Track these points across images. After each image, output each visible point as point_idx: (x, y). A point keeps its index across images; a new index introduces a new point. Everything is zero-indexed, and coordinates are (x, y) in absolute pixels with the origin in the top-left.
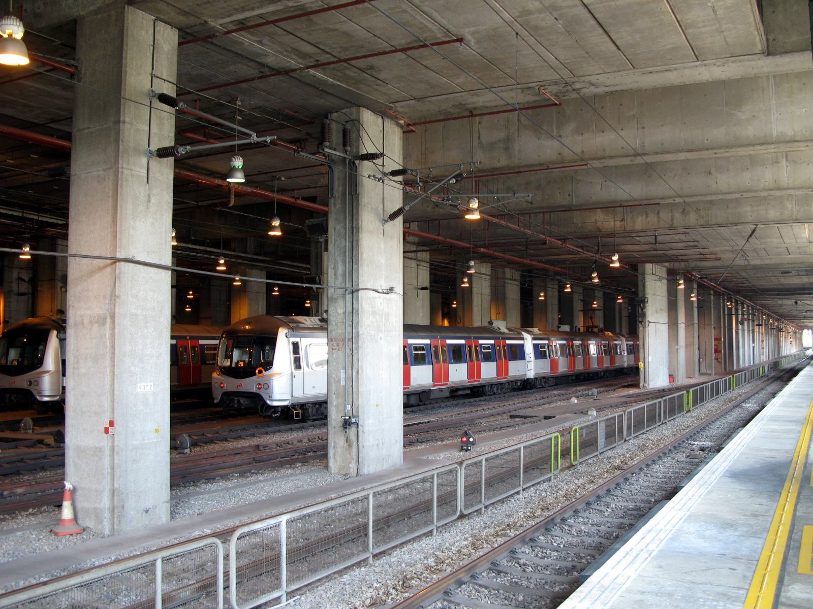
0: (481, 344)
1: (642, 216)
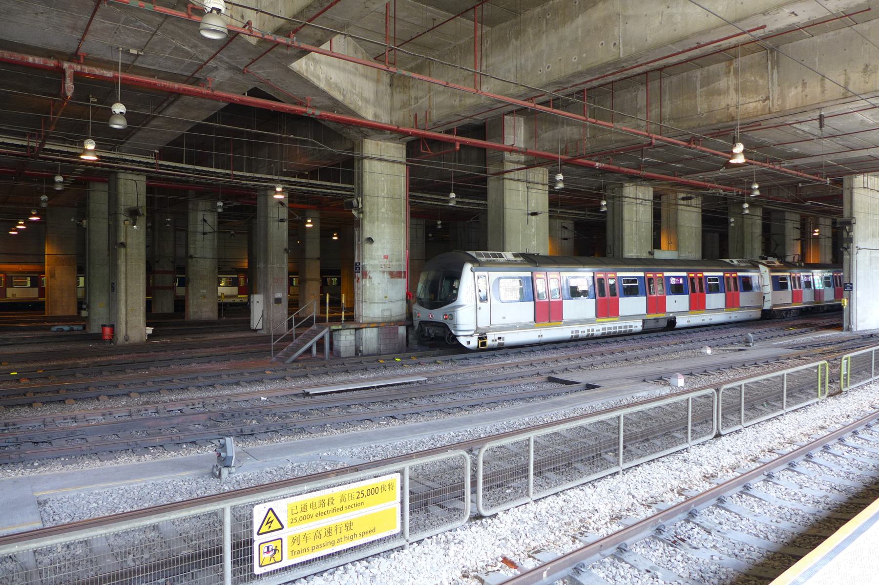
0: (706, 277)
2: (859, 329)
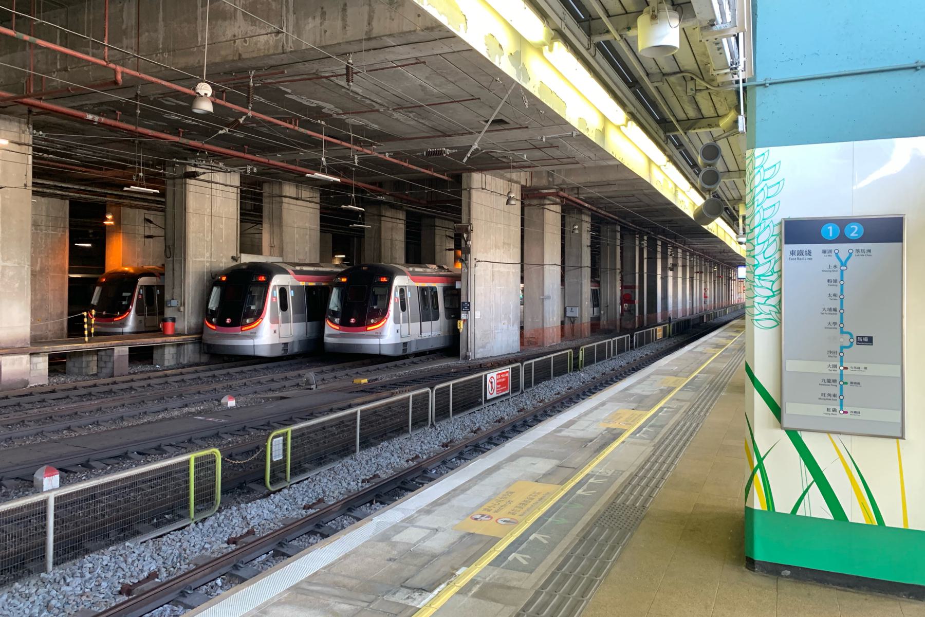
1: (314, 18)
2: (478, 356)
